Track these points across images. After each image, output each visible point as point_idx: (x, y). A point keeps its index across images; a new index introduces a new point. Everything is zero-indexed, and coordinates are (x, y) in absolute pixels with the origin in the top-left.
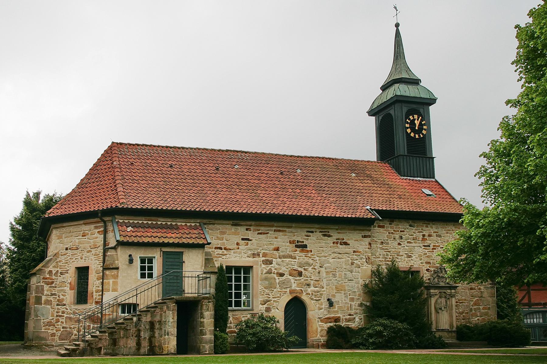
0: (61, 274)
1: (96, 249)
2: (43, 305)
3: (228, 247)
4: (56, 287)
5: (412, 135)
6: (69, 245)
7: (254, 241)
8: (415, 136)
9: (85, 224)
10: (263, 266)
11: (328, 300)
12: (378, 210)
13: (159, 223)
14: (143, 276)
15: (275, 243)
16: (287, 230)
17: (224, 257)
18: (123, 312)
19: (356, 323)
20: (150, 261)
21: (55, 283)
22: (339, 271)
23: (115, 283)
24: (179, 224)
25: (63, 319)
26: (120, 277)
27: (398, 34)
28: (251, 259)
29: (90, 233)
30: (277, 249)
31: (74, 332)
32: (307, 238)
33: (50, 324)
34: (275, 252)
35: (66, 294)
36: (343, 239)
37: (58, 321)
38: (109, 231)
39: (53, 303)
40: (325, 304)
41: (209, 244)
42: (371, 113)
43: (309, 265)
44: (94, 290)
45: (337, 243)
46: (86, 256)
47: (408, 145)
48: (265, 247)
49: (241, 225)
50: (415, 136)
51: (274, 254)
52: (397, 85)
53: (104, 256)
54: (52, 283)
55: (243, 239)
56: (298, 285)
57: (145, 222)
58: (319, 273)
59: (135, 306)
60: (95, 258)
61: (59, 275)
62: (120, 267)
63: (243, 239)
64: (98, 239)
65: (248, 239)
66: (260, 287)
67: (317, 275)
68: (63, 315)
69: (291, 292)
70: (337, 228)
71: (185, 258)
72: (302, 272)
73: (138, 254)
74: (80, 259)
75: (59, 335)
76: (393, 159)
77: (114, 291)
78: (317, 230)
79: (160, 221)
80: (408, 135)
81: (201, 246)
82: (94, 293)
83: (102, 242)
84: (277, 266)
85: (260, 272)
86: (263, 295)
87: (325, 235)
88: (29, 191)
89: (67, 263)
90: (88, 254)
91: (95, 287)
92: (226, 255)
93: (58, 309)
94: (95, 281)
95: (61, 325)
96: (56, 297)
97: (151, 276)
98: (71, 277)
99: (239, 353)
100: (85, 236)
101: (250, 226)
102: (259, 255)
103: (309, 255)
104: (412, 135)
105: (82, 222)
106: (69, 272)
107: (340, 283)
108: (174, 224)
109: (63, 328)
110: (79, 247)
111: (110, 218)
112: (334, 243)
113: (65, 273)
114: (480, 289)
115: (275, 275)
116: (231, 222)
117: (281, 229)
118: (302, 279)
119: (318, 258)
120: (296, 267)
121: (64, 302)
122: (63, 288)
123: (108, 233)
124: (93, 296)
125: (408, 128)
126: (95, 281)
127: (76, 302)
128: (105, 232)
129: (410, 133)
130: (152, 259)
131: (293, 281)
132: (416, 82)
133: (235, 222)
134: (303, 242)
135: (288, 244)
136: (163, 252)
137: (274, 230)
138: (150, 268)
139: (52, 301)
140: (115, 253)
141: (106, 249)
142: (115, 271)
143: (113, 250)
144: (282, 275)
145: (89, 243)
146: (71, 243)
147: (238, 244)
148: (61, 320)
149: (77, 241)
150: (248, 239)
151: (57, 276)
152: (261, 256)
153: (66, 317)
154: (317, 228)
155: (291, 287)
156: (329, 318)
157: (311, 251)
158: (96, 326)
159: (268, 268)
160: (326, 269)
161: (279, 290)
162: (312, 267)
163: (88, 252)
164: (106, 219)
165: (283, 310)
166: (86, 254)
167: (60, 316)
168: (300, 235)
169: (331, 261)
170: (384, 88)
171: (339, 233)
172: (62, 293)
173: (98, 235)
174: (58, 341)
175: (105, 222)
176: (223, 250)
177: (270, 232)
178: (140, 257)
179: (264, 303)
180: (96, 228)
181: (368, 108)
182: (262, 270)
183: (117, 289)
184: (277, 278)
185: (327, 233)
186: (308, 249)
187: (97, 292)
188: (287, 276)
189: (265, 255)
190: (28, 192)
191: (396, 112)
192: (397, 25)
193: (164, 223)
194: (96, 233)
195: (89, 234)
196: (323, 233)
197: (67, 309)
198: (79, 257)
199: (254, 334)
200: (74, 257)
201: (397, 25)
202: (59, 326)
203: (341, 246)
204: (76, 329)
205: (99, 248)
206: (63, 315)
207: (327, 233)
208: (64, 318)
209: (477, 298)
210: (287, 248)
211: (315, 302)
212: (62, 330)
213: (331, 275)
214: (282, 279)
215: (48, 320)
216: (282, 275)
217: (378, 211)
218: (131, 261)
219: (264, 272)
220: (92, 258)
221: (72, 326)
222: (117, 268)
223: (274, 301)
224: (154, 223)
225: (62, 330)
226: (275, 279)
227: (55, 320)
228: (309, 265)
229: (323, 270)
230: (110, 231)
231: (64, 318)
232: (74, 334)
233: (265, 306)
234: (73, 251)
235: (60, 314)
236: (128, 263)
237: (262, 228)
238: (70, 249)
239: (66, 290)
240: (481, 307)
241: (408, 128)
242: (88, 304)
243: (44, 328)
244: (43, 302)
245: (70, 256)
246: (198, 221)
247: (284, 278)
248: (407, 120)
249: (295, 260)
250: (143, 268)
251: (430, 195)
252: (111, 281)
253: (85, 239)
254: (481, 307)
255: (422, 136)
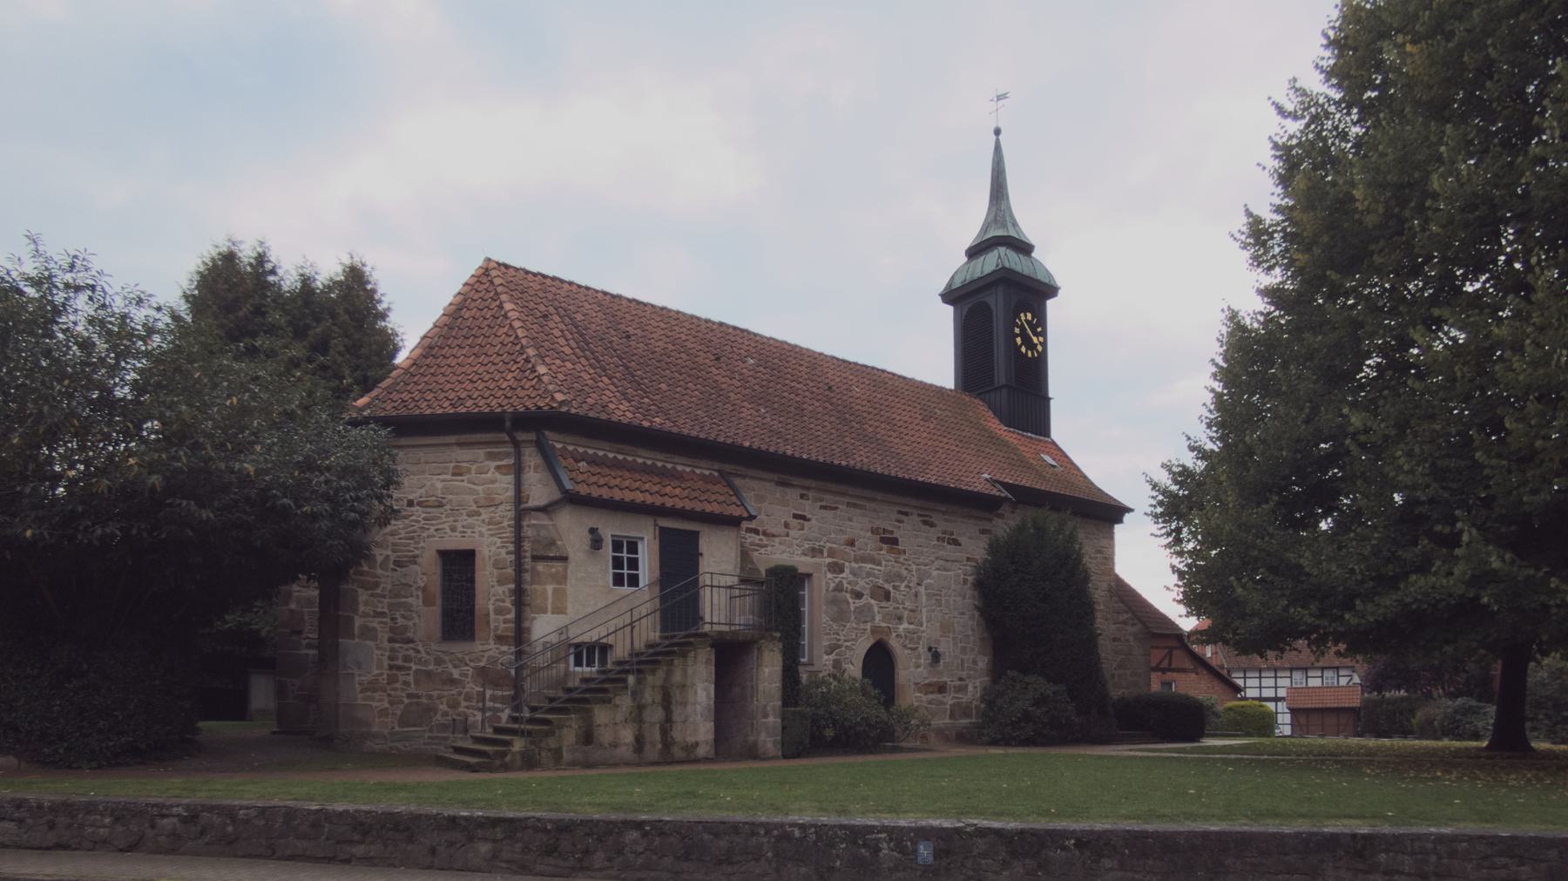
0: (398, 564)
1: (492, 509)
2: (357, 640)
3: (770, 530)
4: (384, 597)
6: (418, 495)
7: (813, 522)
9: (461, 445)
10: (830, 575)
11: (930, 649)
12: (1007, 483)
13: (640, 460)
14: (618, 580)
15: (848, 530)
16: (868, 505)
17: (763, 551)
18: (578, 663)
19: (969, 695)
20: (633, 547)
21: (382, 585)
22: (945, 595)
23: (560, 595)
24: (680, 468)
25: (409, 674)
26: (571, 580)
27: (998, 148)
28: (809, 559)
29: (473, 467)
30: (851, 543)
31: (441, 707)
33: (372, 687)
34: (848, 549)
35: (414, 615)
36: (952, 534)
37: (392, 680)
38: (527, 468)
39: (380, 635)
40: (925, 659)
41: (751, 518)
42: (950, 296)
43: (901, 578)
44: (491, 607)
45: (943, 540)
46: (465, 523)
48: (833, 536)
49: (793, 486)
51: (846, 553)
52: (1002, 250)
53: (518, 527)
54: (377, 585)
55: (796, 516)
56: (884, 617)
57: (611, 455)
58: (916, 596)
59: (605, 649)
60: (490, 530)
61: (392, 566)
62: (571, 555)
63: (796, 516)
64: (496, 485)
65: (803, 518)
66: (825, 618)
67: (913, 598)
68: (406, 664)
69: (875, 630)
70: (944, 509)
72: (889, 592)
73: (611, 528)
74: (448, 530)
75: (399, 712)
76: (989, 391)
77: (558, 613)
78: (916, 512)
79: (640, 456)
81: (733, 522)
82: (492, 616)
83: (511, 493)
84: (851, 578)
85: (824, 588)
86: (828, 634)
87: (925, 523)
89: (412, 538)
90: (470, 520)
91: (492, 601)
92: (766, 546)
93: (392, 650)
94: (493, 586)
95: (403, 690)
96: (384, 620)
97: (634, 581)
98: (427, 572)
99: (1168, 742)
100: (461, 475)
101: (808, 488)
102: (821, 552)
103: (901, 560)
105: (452, 439)
106: (419, 560)
107: (947, 617)
108: (669, 466)
109: (410, 696)
110: (444, 501)
111: (532, 436)
112: (938, 539)
113: (410, 562)
114: (1127, 641)
115: (848, 596)
116: (775, 477)
117: (858, 503)
118: (890, 605)
119: (914, 567)
120: (880, 582)
121: (410, 635)
122: (404, 600)
123: (526, 471)
124: (488, 623)
126: (493, 586)
127: (444, 633)
128: (518, 470)
130: (695, 536)
131: (876, 609)
132: (1024, 248)
133: (784, 477)
134: (892, 532)
135: (869, 534)
136: (661, 528)
137: (848, 503)
138: (634, 564)
139: (377, 630)
140: (550, 523)
141: (523, 510)
142: (558, 566)
143: (540, 515)
144: (859, 595)
145: (473, 492)
146: (423, 491)
147: (786, 525)
148: (402, 678)
149: (439, 485)
150: (803, 518)
151: (386, 570)
152: (825, 554)
153: (417, 672)
154: (915, 507)
155: (873, 619)
156: (930, 685)
157: (905, 552)
158: (500, 693)
159: (837, 580)
160: (926, 589)
161: (855, 626)
162: (905, 583)
163: (470, 515)
164: (521, 436)
165: (861, 665)
166: (464, 520)
167: (400, 668)
168: (886, 518)
169: (935, 573)
170: (974, 252)
171: (946, 520)
172: (403, 612)
173: (498, 475)
174: (397, 729)
175: (517, 444)
176: (761, 537)
177: (840, 507)
178: (612, 536)
179: (831, 649)
180: (491, 456)
181: (941, 286)
182: (827, 582)
183: (566, 608)
184: (851, 601)
185: (928, 519)
186: (900, 547)
187: (499, 611)
188: (866, 599)
189: (832, 553)
190: (1249, 214)
191: (996, 301)
192: (997, 132)
193: (649, 462)
194: (492, 470)
195: (473, 472)
196: (925, 519)
197: (418, 652)
198: (446, 526)
200: (432, 525)
201: (997, 132)
202: (399, 693)
203: (949, 547)
204: (445, 700)
205: (501, 508)
206: (406, 664)
207: (928, 519)
208: (411, 672)
209: (18, 704)
210: (868, 543)
211: (909, 652)
212: (406, 701)
213: (933, 602)
214: (860, 603)
215: (369, 677)
216: (859, 595)
217: (1006, 486)
218: (596, 543)
219: (831, 588)
220: (483, 530)
221: (435, 693)
222: (564, 559)
223: (847, 647)
224: (630, 459)
225: (406, 701)
226: (848, 603)
227: (385, 676)
228: (901, 578)
229: (922, 589)
230: (530, 467)
231: (411, 672)
232: (440, 712)
233: (832, 657)
234: (429, 510)
235: (399, 662)
236: (587, 548)
237: (827, 497)
238: (420, 504)
239: (411, 605)
240: (1128, 672)
242: (478, 642)
243: (360, 696)
244: (356, 631)
245: (419, 522)
246: (716, 466)
247: (862, 602)
249: (878, 568)
250: (617, 563)
251: (1054, 466)
252: (550, 588)
253: (463, 483)
254: (1128, 672)
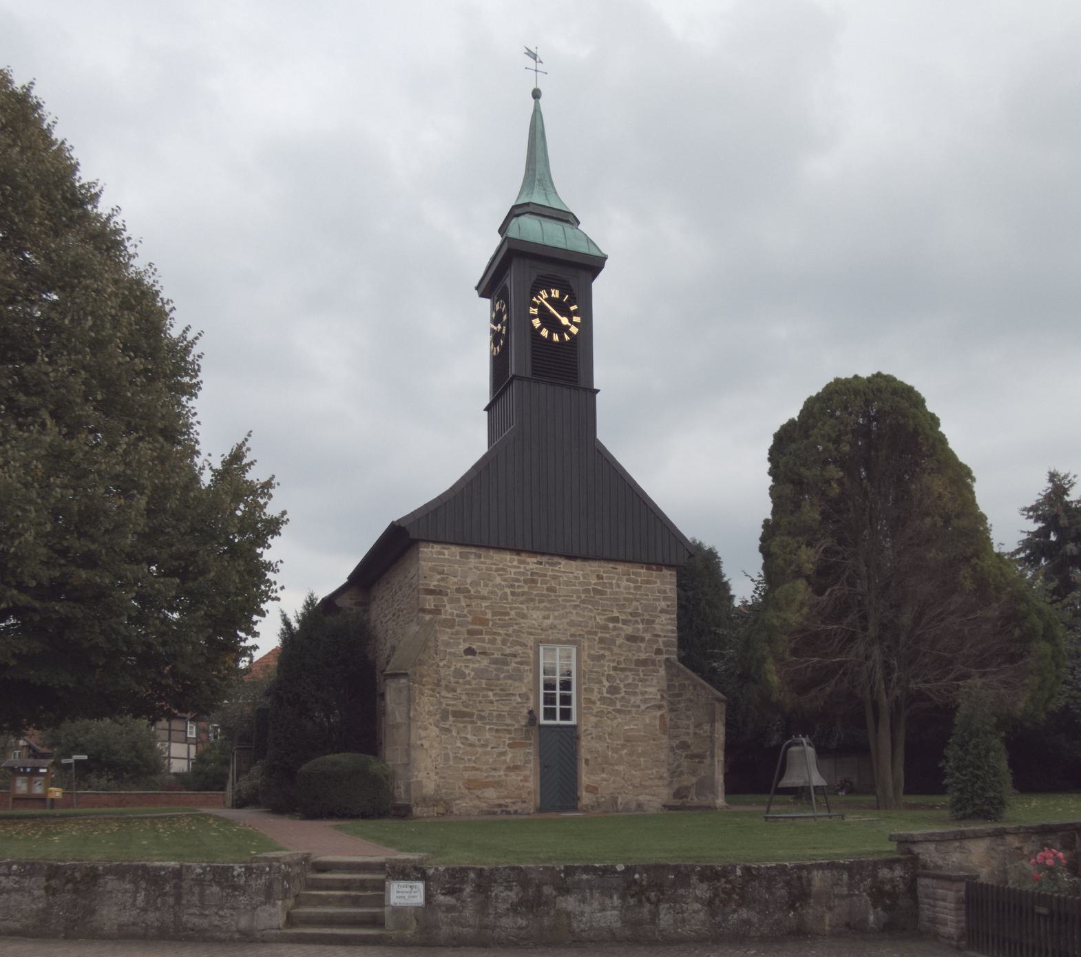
5: (545, 333)
8: (550, 336)
27: (537, 112)
32: (530, 630)
47: (575, 372)
50: (550, 336)
71: (815, 784)
80: (536, 332)
88: (286, 611)
104: (545, 333)
125: (534, 317)
129: (540, 328)
132: (566, 218)
192: (536, 94)
199: (79, 824)
201: (536, 94)
241: (534, 317)
248: (534, 299)
255: (567, 338)
